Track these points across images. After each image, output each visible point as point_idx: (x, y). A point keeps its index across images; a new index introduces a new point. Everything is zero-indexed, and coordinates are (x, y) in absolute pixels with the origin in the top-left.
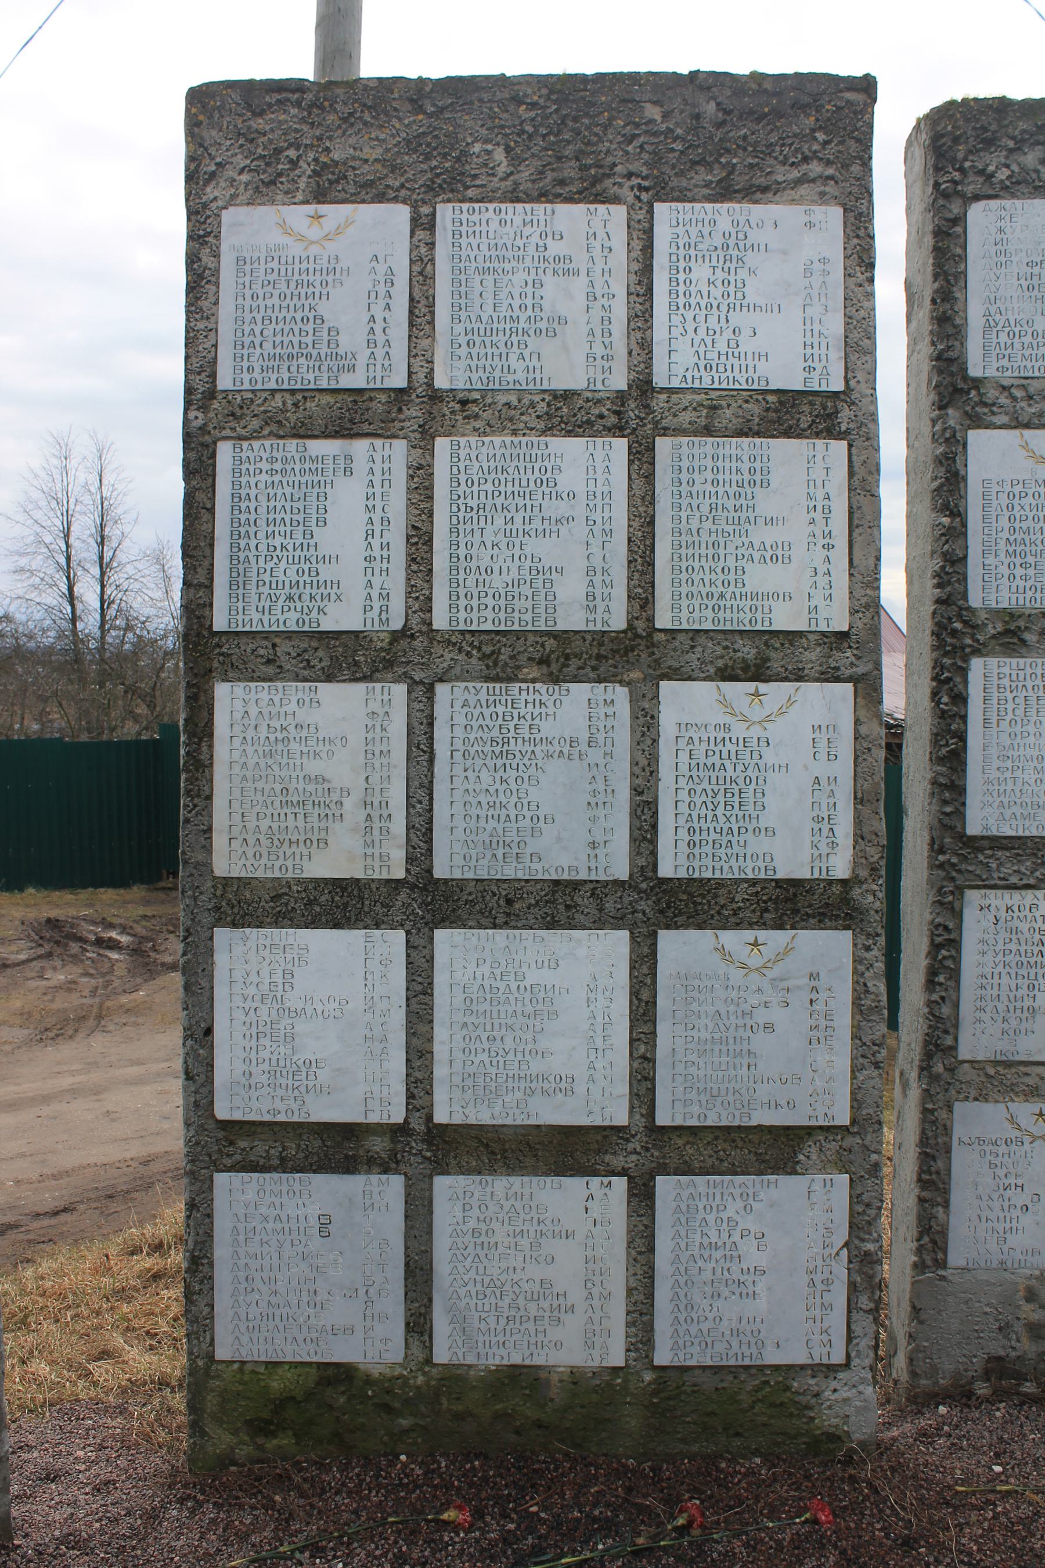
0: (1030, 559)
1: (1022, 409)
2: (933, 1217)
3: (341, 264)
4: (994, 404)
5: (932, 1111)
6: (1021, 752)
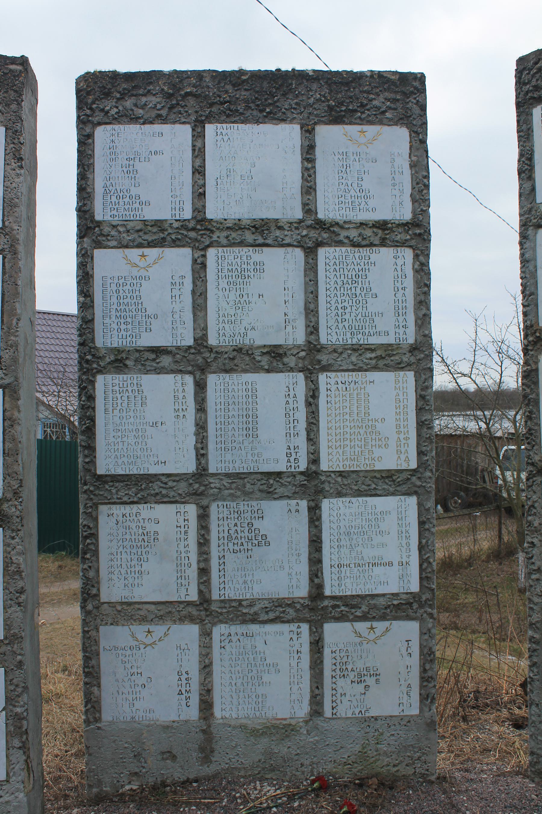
0: (129, 320)
1: (123, 237)
2: (92, 693)
4: (108, 235)
5: (88, 632)
6: (127, 427)
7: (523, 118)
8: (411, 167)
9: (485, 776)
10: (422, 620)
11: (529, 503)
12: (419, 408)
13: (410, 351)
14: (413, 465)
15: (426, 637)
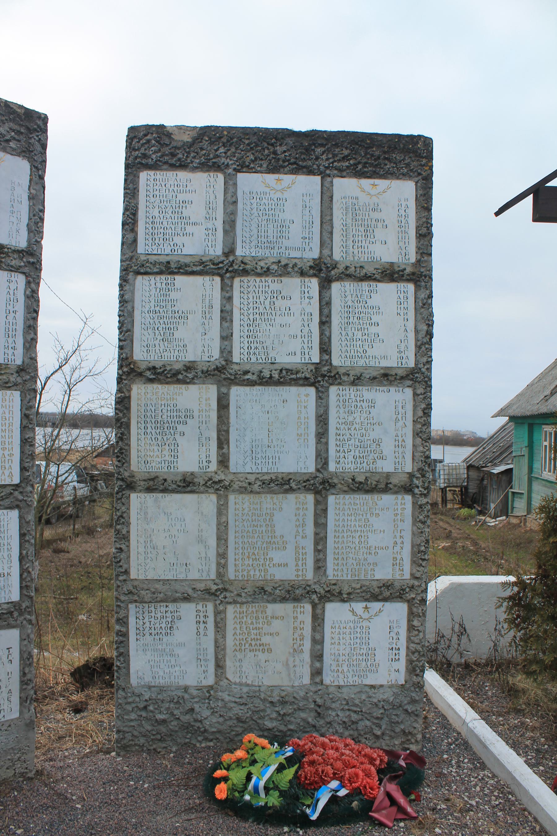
7: (130, 178)
8: (29, 199)
9: (71, 761)
10: (21, 627)
11: (118, 514)
12: (23, 426)
13: (17, 372)
14: (16, 480)
15: (26, 642)
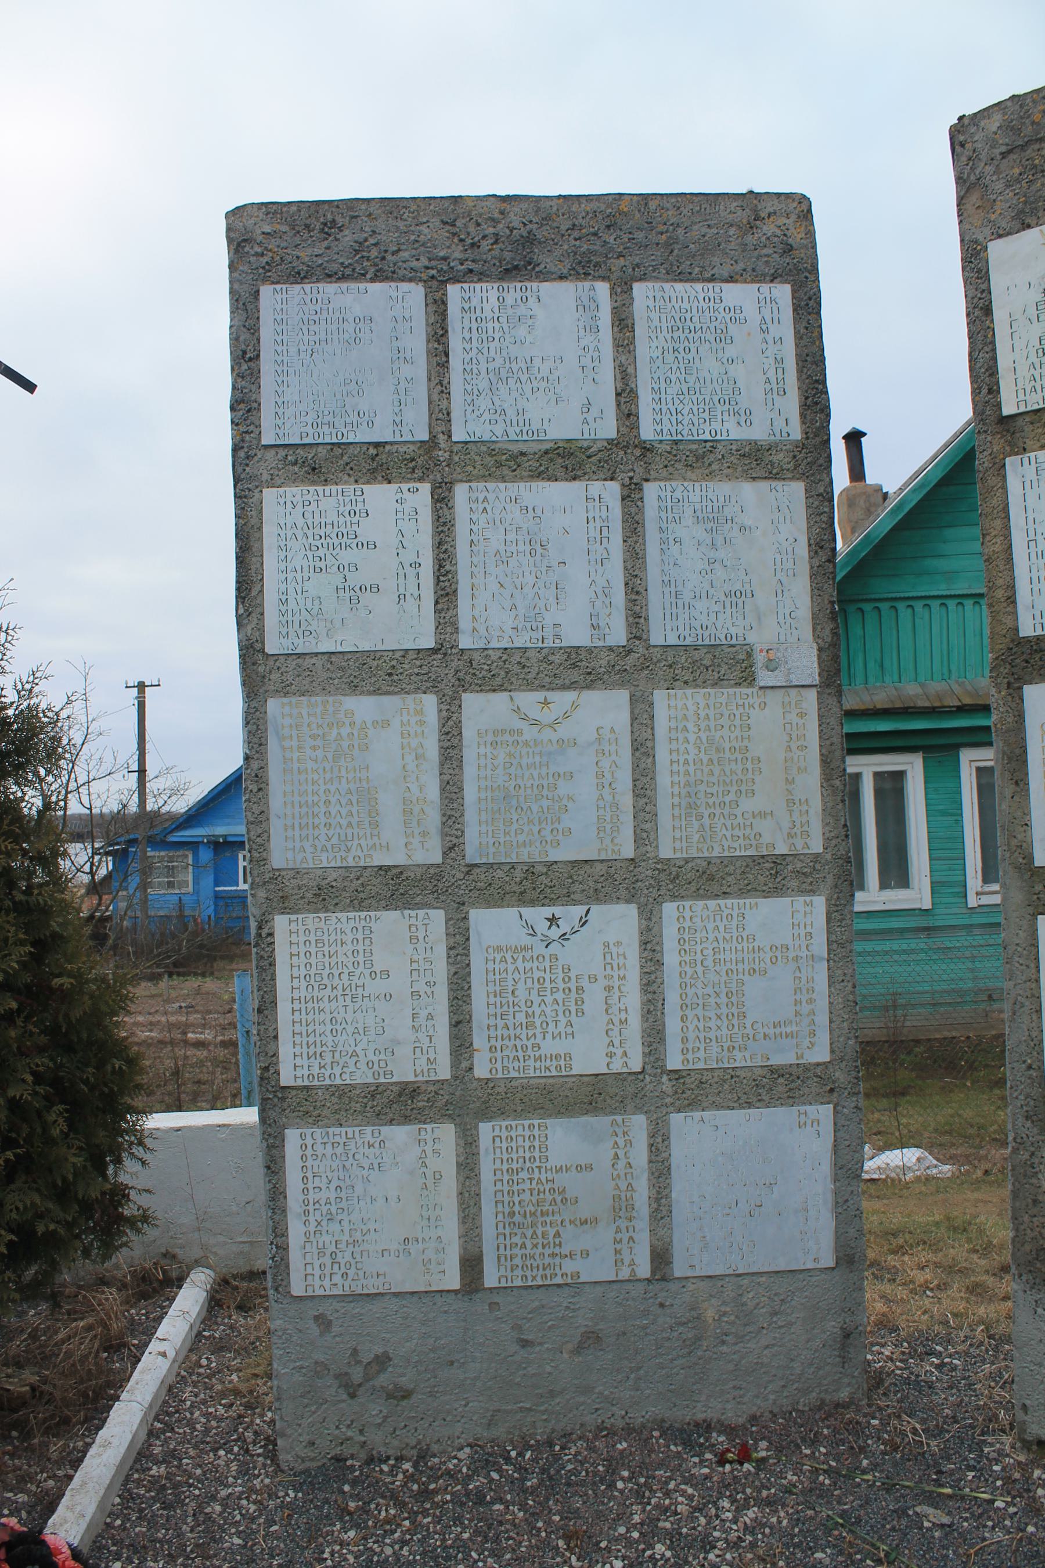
3: (361, 355)
